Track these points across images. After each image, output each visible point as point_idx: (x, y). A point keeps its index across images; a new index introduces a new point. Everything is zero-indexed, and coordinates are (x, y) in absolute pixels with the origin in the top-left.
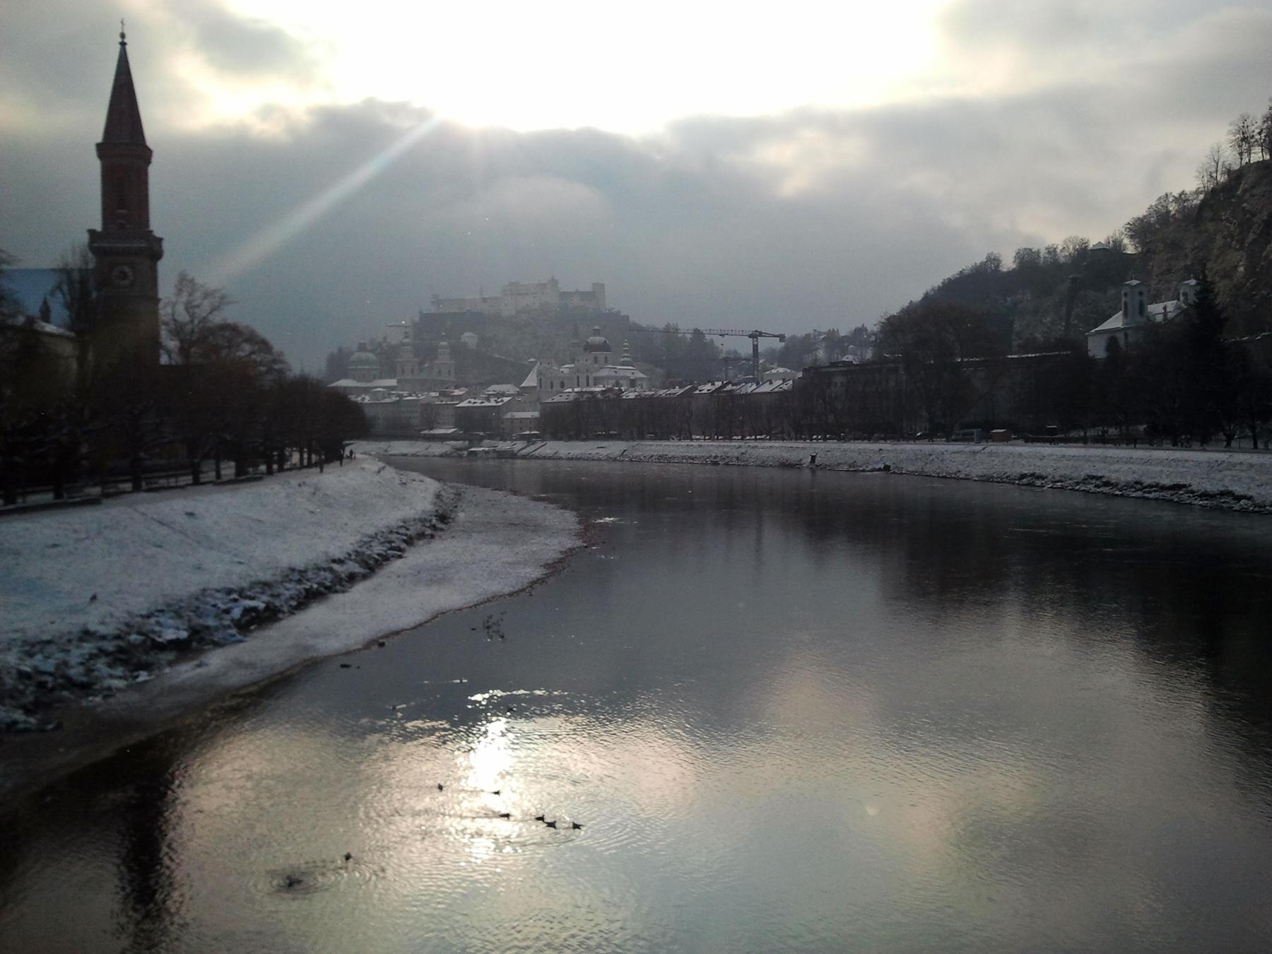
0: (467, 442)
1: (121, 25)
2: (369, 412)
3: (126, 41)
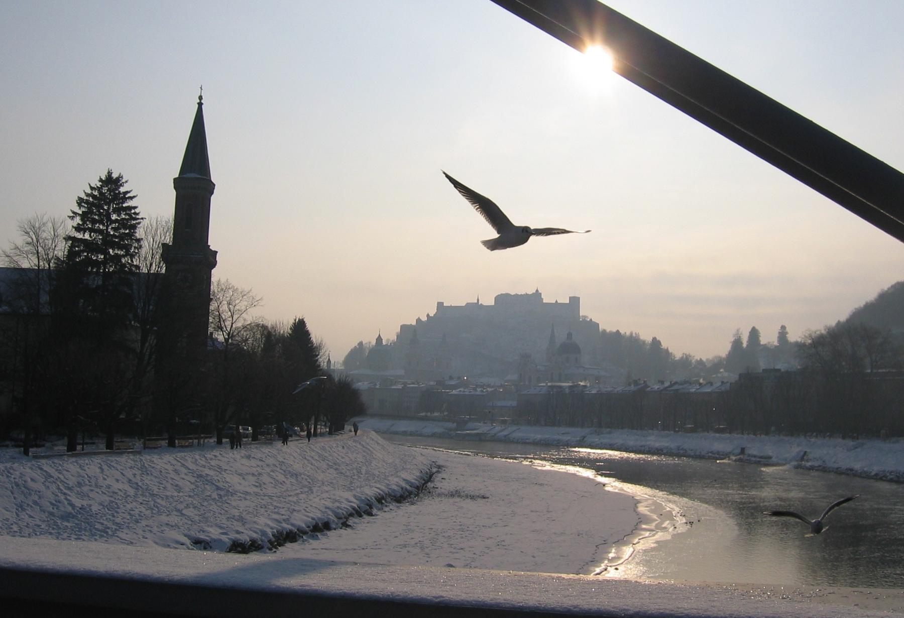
0: (455, 424)
1: (200, 89)
2: (364, 398)
3: (202, 101)
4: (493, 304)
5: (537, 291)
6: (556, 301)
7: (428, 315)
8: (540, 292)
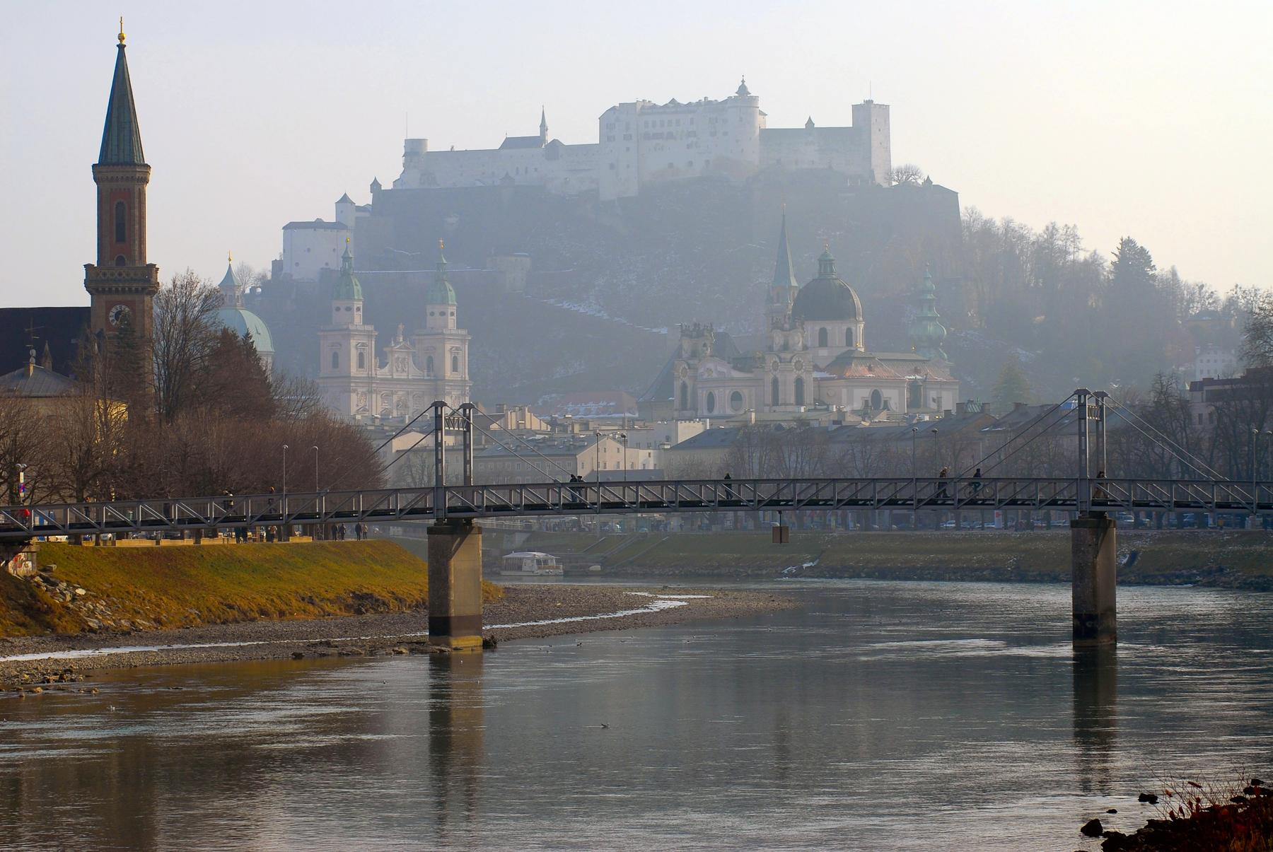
4: (597, 142)
5: (743, 89)
6: (810, 122)
7: (375, 186)
8: (753, 92)
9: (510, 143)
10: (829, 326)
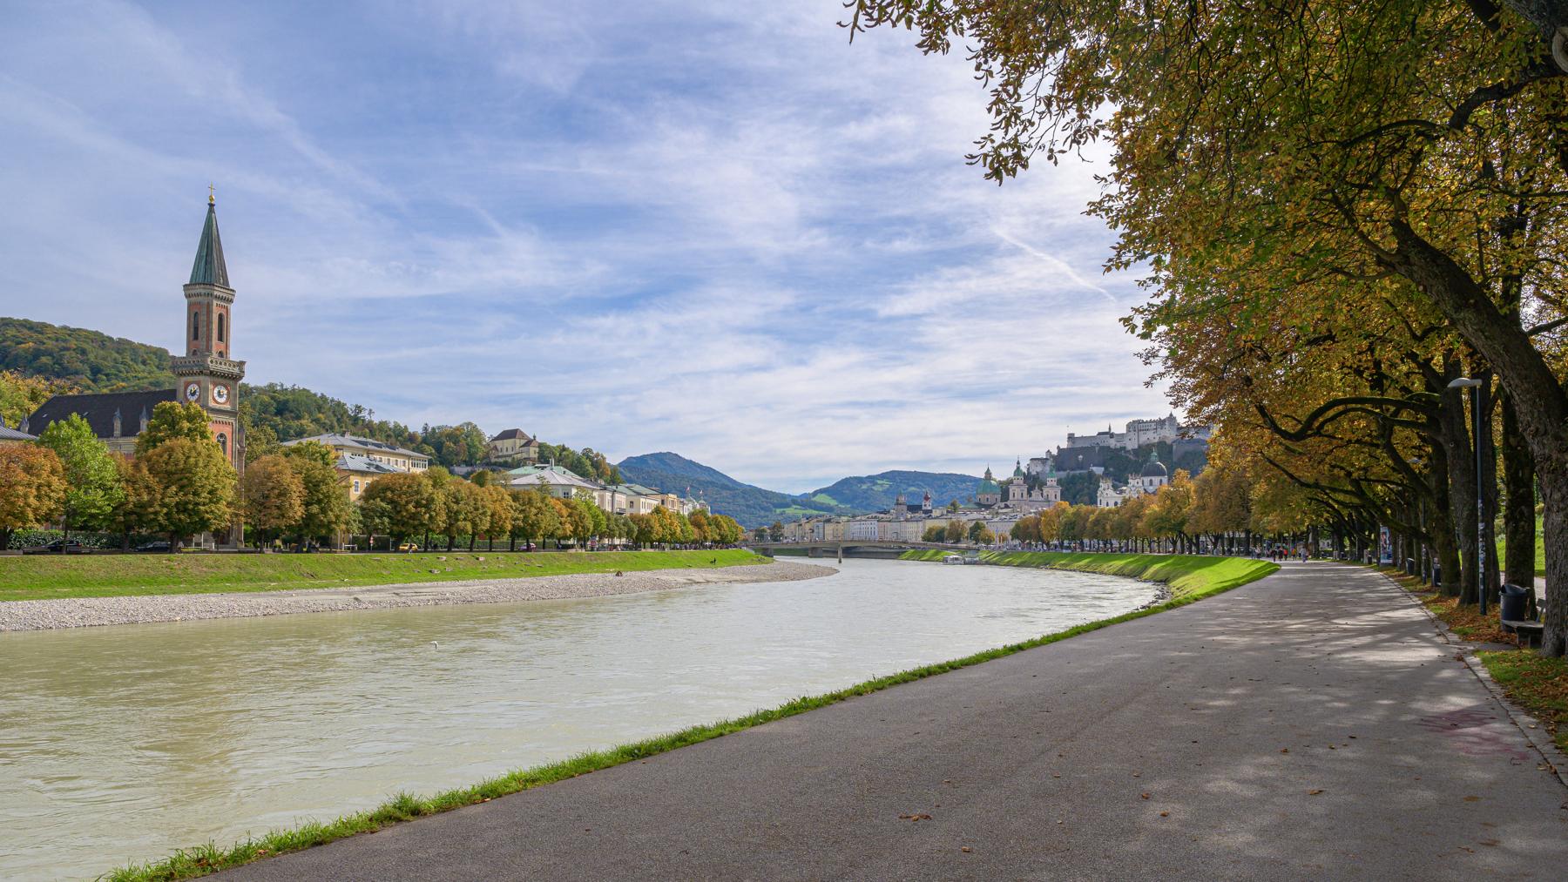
9: (1099, 434)
10: (1153, 478)
